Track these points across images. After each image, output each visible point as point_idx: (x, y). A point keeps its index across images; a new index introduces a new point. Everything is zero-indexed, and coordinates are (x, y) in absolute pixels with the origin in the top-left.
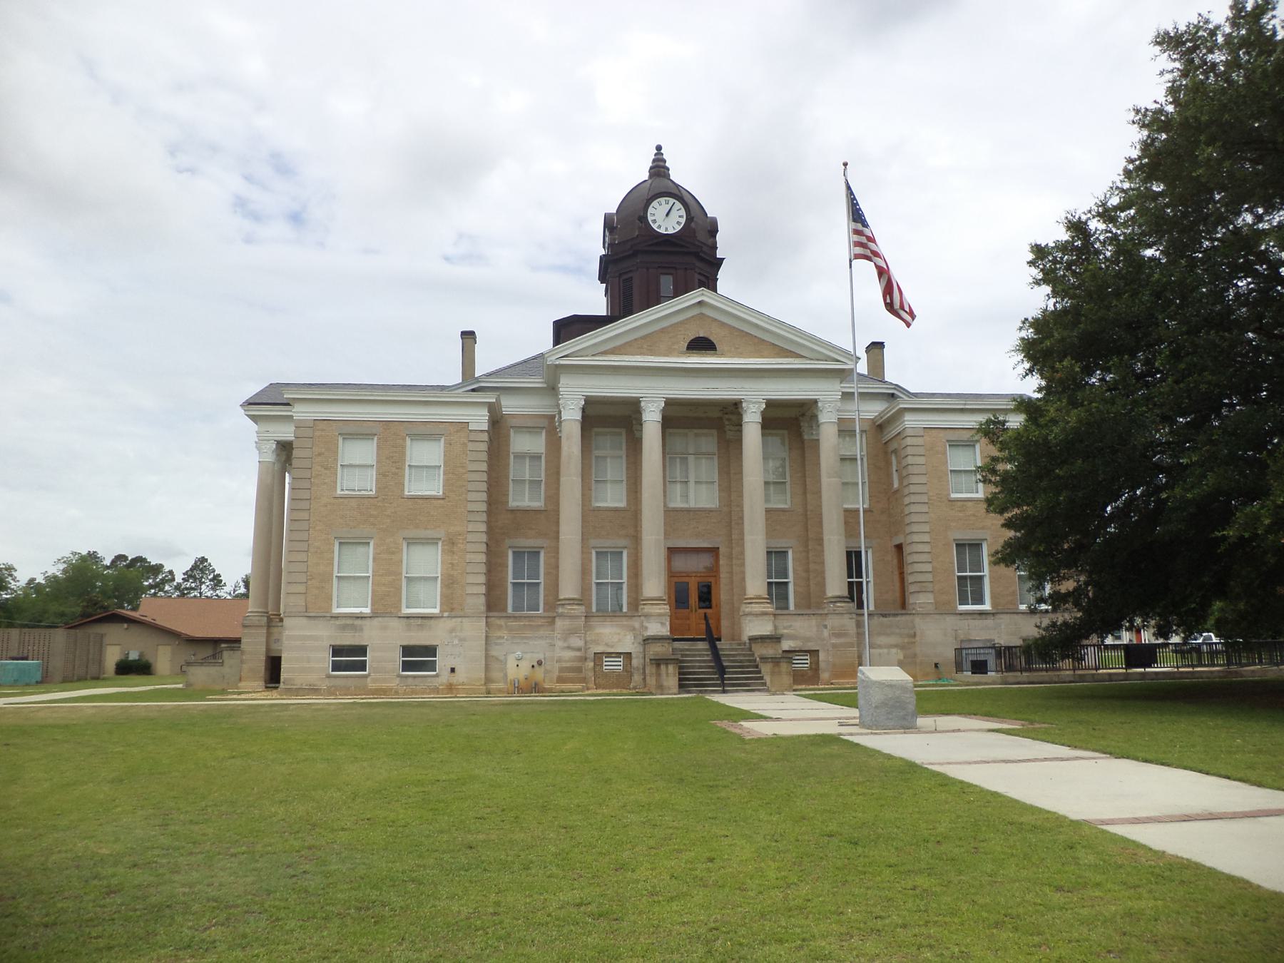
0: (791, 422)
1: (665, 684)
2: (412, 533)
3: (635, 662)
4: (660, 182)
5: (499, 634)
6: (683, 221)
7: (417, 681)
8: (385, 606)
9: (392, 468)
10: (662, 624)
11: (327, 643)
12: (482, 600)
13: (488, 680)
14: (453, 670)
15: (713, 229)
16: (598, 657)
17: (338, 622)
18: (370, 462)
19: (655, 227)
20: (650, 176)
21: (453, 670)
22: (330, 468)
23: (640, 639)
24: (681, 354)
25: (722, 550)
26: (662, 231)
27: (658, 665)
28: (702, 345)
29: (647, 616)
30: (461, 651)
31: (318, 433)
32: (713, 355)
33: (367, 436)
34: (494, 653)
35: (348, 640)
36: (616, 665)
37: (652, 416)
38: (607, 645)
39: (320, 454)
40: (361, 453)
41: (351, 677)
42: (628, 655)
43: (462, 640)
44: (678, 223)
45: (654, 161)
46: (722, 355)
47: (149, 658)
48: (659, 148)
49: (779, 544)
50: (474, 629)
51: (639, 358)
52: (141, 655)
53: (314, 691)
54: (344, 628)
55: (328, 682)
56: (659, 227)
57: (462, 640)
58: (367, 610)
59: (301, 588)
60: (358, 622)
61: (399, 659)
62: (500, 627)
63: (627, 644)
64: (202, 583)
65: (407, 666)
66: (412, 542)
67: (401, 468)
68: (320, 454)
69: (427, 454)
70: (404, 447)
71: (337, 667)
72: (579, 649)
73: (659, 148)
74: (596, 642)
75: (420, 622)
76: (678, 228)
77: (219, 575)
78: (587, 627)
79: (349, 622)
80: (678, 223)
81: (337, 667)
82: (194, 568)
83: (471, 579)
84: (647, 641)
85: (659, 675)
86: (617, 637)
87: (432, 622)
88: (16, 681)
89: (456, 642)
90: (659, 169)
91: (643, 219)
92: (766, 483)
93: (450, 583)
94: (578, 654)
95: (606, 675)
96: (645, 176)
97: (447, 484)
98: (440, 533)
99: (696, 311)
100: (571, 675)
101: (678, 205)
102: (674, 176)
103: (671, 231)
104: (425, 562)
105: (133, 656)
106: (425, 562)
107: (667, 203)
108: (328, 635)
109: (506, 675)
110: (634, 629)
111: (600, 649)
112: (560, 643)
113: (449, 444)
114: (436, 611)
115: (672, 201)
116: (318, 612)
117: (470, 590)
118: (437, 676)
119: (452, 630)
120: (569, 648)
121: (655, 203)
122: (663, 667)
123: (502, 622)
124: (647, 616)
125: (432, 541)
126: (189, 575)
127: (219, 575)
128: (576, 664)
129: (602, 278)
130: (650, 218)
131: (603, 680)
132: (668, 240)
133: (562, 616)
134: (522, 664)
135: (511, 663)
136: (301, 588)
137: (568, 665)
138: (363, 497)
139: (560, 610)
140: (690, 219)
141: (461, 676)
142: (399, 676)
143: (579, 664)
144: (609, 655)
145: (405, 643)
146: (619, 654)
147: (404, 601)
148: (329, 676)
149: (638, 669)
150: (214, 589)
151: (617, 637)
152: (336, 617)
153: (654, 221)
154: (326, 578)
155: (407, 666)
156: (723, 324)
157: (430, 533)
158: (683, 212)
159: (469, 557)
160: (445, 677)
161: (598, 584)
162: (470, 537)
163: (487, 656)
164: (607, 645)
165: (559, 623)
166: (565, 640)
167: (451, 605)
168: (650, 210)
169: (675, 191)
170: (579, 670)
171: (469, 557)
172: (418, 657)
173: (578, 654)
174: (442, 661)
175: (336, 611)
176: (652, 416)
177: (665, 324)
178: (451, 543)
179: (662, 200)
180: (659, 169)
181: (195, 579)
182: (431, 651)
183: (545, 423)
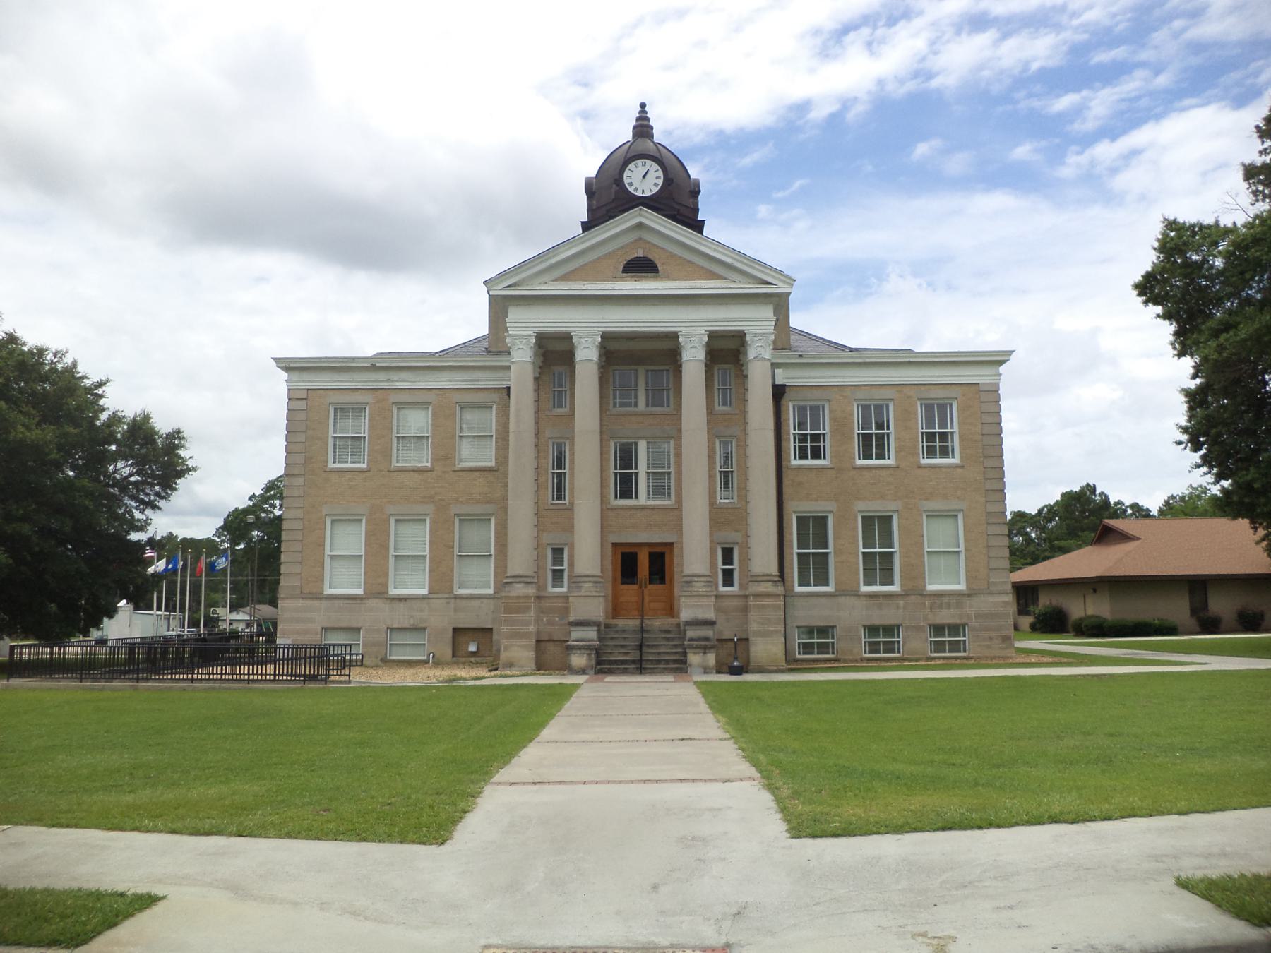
0: (726, 353)
6: (660, 182)
15: (695, 191)
19: (631, 189)
20: (634, 136)
33: (424, 405)
40: (417, 422)
44: (656, 184)
45: (638, 119)
48: (643, 105)
56: (636, 189)
58: (360, 591)
66: (933, 515)
73: (643, 105)
76: (655, 190)
80: (656, 184)
90: (643, 128)
91: (619, 181)
107: (644, 165)
115: (649, 162)
121: (632, 166)
129: (1063, 495)
130: (626, 182)
140: (668, 181)
147: (652, 368)
153: (631, 184)
158: (660, 173)
161: (554, 571)
168: (627, 173)
175: (328, 591)
179: (639, 162)
180: (643, 128)
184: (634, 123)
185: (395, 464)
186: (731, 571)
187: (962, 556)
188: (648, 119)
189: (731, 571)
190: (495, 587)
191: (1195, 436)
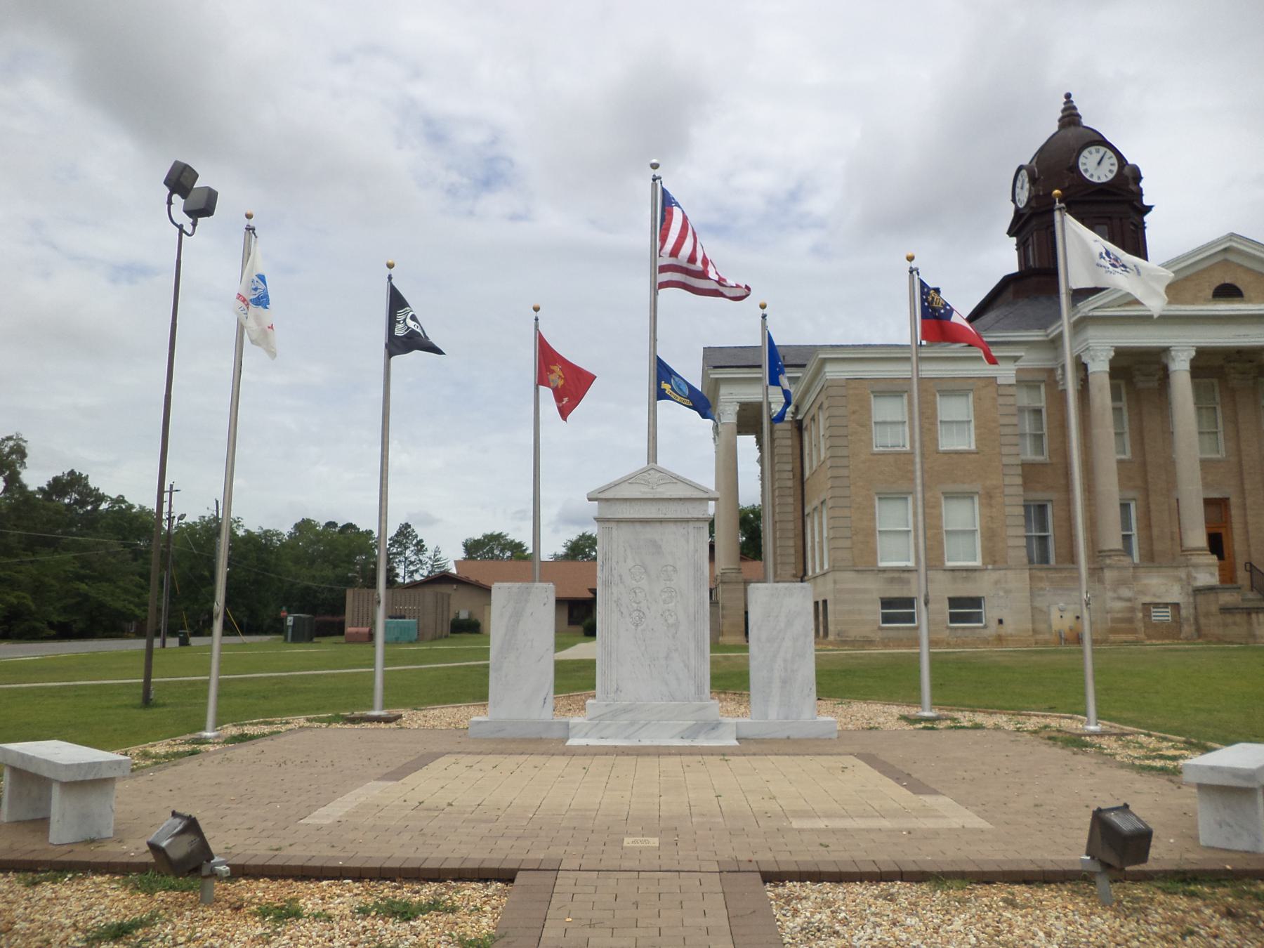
1: (1258, 632)
2: (950, 487)
3: (1184, 613)
4: (1071, 131)
5: (1042, 585)
6: (1115, 169)
7: (967, 633)
8: (933, 557)
9: (928, 422)
10: (1212, 574)
11: (876, 596)
12: (1023, 552)
13: (1035, 631)
14: (1001, 622)
15: (1136, 176)
16: (1146, 606)
17: (886, 575)
18: (900, 419)
19: (1087, 176)
21: (1001, 622)
22: (865, 424)
23: (1190, 589)
24: (1207, 301)
25: (1234, 500)
26: (1095, 180)
27: (1249, 614)
28: (1227, 292)
29: (1196, 566)
30: (1009, 602)
31: (851, 392)
32: (1240, 302)
34: (1037, 604)
35: (895, 592)
36: (1164, 616)
37: (1180, 366)
38: (1154, 595)
39: (854, 412)
40: (886, 410)
41: (898, 629)
42: (1176, 606)
43: (1007, 592)
45: (1063, 111)
46: (1250, 301)
47: (477, 617)
48: (1068, 96)
49: (1039, 496)
50: (1018, 580)
51: (1183, 307)
52: (470, 614)
53: (869, 642)
54: (892, 580)
55: (880, 633)
56: (1092, 176)
57: (1007, 592)
59: (848, 543)
60: (906, 575)
61: (879, 611)
62: (1041, 579)
63: (1175, 594)
64: (406, 548)
65: (954, 618)
66: (950, 496)
67: (934, 424)
68: (854, 412)
69: (953, 409)
70: (935, 403)
71: (887, 619)
72: (1129, 600)
73: (1068, 96)
74: (1144, 593)
75: (964, 574)
76: (1111, 176)
77: (421, 541)
78: (1135, 578)
79: (896, 575)
80: (1111, 171)
81: (887, 619)
82: (400, 533)
83: (1011, 532)
84: (1198, 591)
85: (1250, 624)
86: (1164, 587)
87: (977, 574)
88: (397, 639)
89: (1001, 593)
90: (1070, 117)
91: (1074, 168)
92: (1201, 433)
93: (991, 537)
94: (1128, 604)
95: (1155, 625)
96: (1054, 127)
97: (979, 438)
98: (977, 487)
99: (1219, 258)
100: (1123, 625)
101: (1110, 153)
102: (1086, 122)
103: (1104, 180)
104: (961, 516)
105: (464, 615)
106: (961, 516)
107: (1098, 151)
108: (876, 589)
109: (1050, 626)
110: (1181, 580)
111: (1148, 599)
112: (1110, 594)
113: (978, 400)
114: (978, 563)
116: (864, 563)
117: (1011, 542)
118: (985, 627)
119: (997, 582)
120: (1120, 599)
121: (1085, 153)
122: (1254, 616)
123: (1043, 574)
124: (1196, 566)
125: (969, 496)
126: (395, 541)
127: (421, 541)
128: (1127, 615)
130: (1082, 168)
131: (1157, 631)
132: (1102, 189)
133: (1110, 566)
134: (1066, 615)
135: (1055, 614)
136: (848, 543)
137: (1119, 615)
138: (899, 453)
139: (1108, 561)
141: (1009, 628)
142: (948, 628)
143: (1129, 615)
144: (1157, 605)
145: (952, 595)
146: (1166, 605)
148: (881, 629)
149: (1187, 619)
150: (416, 554)
151: (1164, 587)
152: (884, 570)
153: (1086, 171)
154: (870, 533)
155: (954, 618)
156: (1249, 270)
157: (966, 487)
158: (1114, 160)
159: (1008, 510)
160: (993, 628)
162: (1007, 491)
163: (1033, 608)
164: (1154, 595)
165: (1109, 575)
166: (1115, 591)
167: (993, 557)
169: (1098, 138)
170: (1130, 621)
171: (1008, 510)
172: (965, 608)
173: (1128, 604)
174: (990, 612)
176: (1180, 366)
177: (1200, 267)
178: (988, 497)
179: (1093, 149)
181: (401, 544)
182: (976, 602)
183: (1043, 376)
184: (1060, 115)
185: (908, 448)
186: (1045, 538)
187: (978, 535)
188: (1075, 108)
189: (1045, 538)
190: (983, 558)
191: (72, 483)
